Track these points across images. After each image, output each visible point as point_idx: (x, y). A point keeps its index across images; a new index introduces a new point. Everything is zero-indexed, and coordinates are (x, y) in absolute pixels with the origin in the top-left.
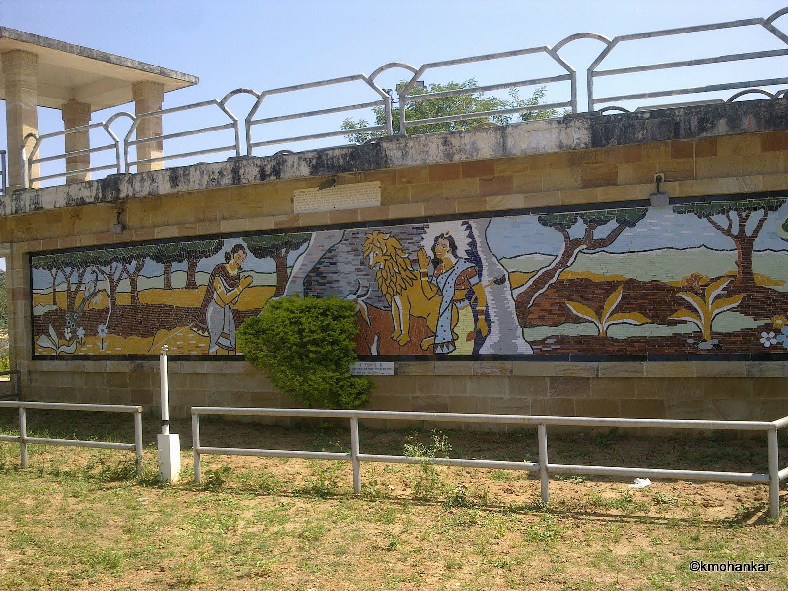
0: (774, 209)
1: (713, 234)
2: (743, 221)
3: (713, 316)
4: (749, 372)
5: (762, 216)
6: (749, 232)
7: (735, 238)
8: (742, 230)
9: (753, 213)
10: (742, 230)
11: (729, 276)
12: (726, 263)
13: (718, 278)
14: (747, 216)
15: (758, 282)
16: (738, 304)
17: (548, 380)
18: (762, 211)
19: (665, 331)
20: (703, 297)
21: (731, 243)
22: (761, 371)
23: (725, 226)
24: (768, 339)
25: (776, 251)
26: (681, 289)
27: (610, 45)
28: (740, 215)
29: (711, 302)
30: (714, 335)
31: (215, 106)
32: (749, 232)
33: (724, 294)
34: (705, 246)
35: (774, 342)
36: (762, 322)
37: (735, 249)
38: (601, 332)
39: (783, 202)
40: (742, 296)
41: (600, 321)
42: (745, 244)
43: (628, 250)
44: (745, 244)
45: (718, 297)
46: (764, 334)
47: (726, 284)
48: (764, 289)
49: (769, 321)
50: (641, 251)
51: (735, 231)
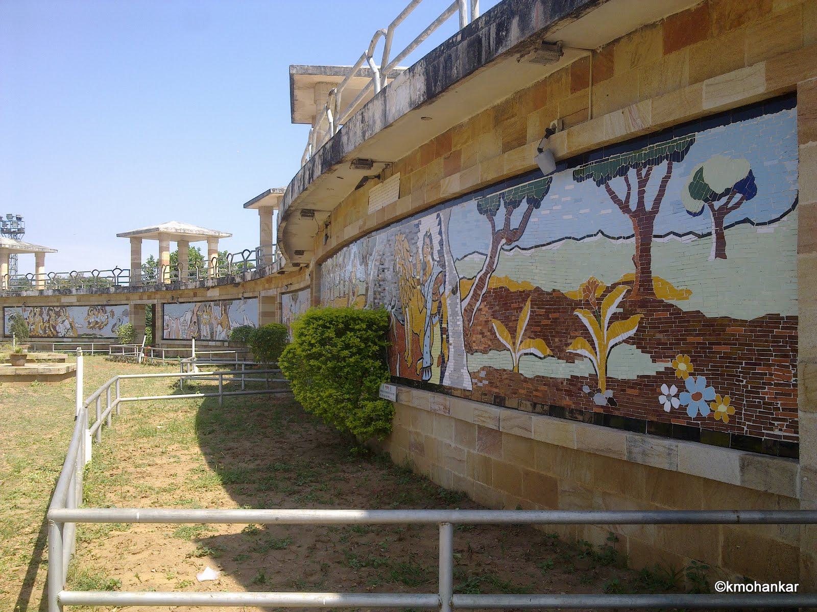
0: (678, 157)
1: (610, 211)
2: (643, 183)
3: (608, 351)
4: (630, 452)
5: (665, 174)
6: (648, 207)
7: (634, 215)
8: (641, 203)
9: (655, 168)
10: (641, 203)
11: (624, 283)
12: (618, 264)
13: (614, 286)
14: (648, 175)
15: (660, 293)
16: (634, 331)
17: (476, 426)
18: (665, 163)
19: (559, 370)
20: (598, 316)
21: (626, 225)
22: (644, 453)
23: (622, 197)
24: (669, 397)
25: (680, 236)
26: (578, 305)
27: (122, 271)
28: (639, 175)
29: (606, 325)
30: (611, 382)
31: (111, 272)
32: (648, 207)
33: (620, 313)
34: (602, 233)
35: (676, 403)
36: (661, 366)
37: (633, 236)
38: (515, 365)
39: (692, 142)
40: (637, 318)
41: (514, 348)
42: (644, 221)
43: (534, 244)
44: (644, 221)
45: (615, 317)
46: (664, 388)
47: (622, 296)
48: (664, 306)
49: (669, 365)
50: (544, 245)
51: (633, 206)
